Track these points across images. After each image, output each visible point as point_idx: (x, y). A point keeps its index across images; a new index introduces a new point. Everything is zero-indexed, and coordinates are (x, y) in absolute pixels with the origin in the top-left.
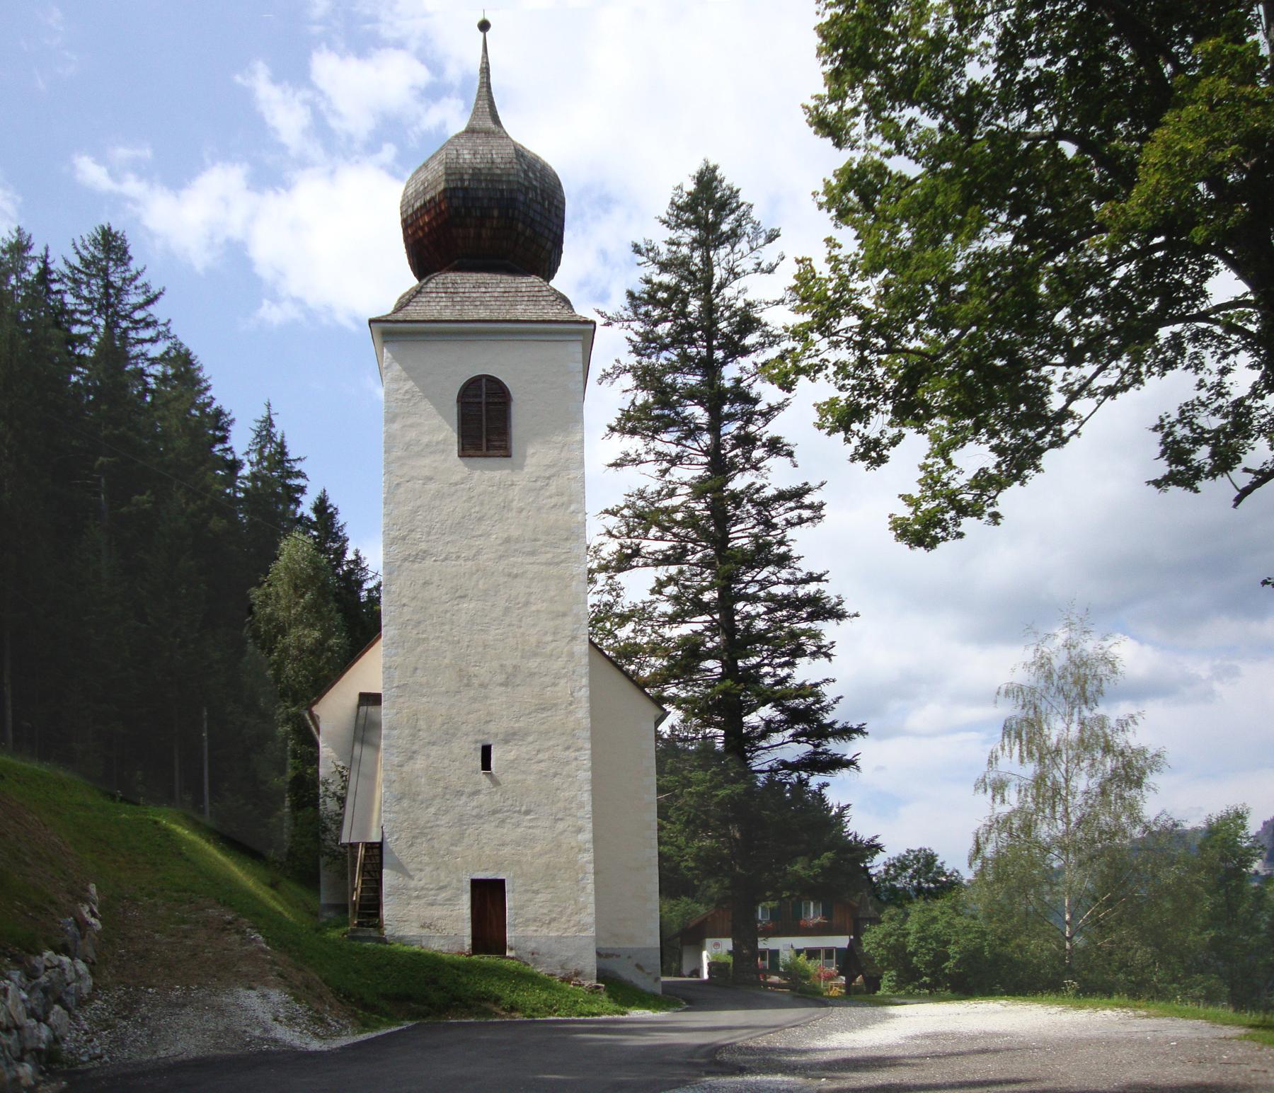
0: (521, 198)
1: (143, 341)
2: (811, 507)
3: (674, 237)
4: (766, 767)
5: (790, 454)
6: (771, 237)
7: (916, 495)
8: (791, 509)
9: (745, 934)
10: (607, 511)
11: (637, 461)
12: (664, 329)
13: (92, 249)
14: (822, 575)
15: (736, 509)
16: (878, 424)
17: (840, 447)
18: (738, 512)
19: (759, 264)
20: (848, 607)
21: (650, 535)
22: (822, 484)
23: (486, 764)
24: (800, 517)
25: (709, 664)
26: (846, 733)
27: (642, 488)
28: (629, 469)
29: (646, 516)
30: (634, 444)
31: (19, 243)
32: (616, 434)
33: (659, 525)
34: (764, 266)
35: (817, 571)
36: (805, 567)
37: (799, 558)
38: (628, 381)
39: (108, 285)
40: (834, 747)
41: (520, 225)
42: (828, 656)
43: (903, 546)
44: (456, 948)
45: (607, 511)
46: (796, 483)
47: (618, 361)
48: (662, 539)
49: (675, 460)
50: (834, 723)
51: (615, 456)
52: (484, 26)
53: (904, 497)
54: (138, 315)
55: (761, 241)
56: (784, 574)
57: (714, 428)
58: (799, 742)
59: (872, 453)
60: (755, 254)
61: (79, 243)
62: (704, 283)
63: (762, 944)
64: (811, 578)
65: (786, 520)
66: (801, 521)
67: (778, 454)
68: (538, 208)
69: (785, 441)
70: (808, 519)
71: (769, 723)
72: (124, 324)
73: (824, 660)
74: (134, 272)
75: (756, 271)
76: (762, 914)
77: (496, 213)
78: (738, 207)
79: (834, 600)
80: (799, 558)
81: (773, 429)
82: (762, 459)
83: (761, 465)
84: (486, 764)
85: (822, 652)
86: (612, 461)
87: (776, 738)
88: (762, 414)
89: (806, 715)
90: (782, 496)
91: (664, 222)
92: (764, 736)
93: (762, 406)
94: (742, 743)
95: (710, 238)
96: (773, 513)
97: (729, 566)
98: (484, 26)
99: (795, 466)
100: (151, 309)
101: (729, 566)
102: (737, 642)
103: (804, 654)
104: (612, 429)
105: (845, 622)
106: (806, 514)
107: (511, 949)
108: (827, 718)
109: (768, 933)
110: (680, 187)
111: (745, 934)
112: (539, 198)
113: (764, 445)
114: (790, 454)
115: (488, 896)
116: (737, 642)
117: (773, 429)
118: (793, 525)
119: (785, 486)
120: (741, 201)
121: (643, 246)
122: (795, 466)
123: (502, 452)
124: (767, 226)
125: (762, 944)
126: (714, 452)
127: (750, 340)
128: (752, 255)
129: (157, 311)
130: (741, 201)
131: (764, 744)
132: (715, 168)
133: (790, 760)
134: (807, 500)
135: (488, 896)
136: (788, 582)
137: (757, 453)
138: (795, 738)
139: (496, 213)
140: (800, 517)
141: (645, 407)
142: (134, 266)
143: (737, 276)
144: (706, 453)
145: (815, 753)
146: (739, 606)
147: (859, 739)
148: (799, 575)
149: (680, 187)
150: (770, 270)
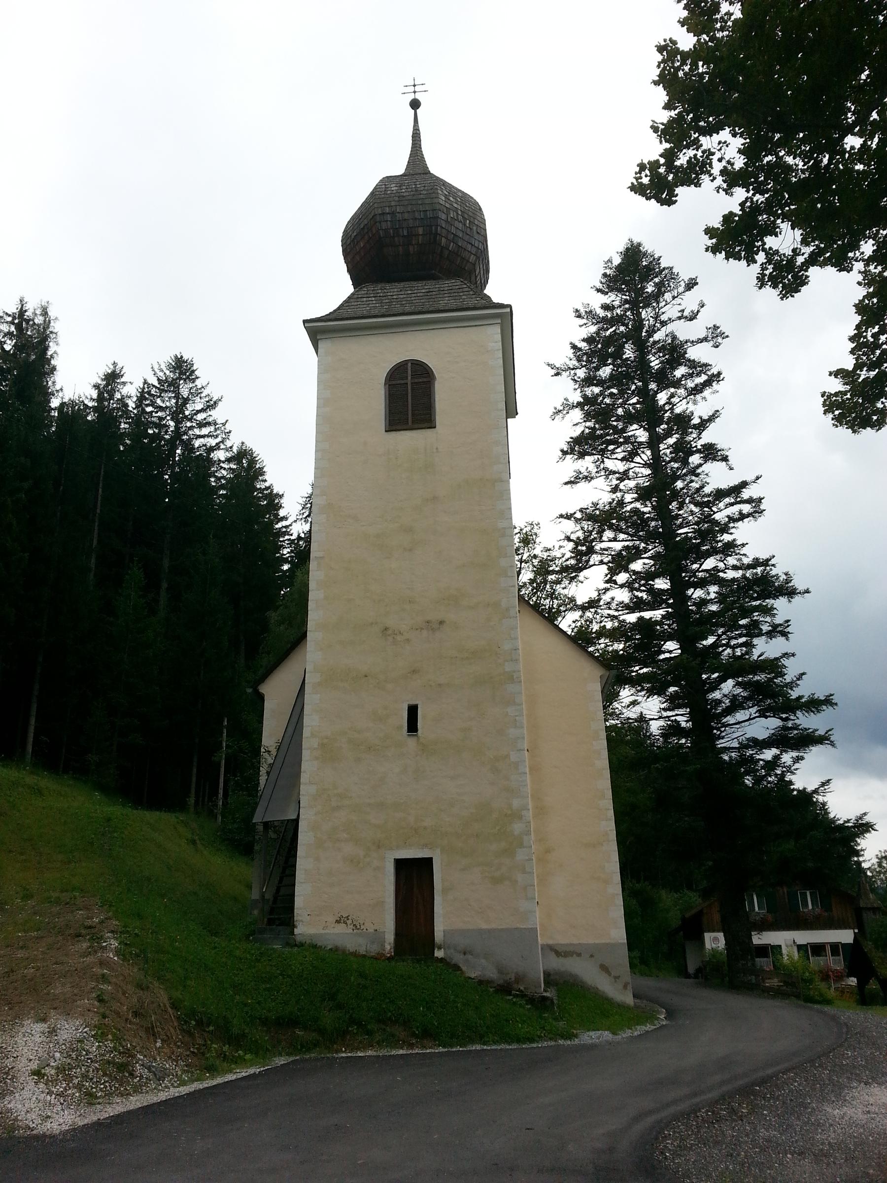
0: (444, 217)
1: (203, 436)
2: (749, 501)
3: (608, 302)
4: (735, 744)
5: (725, 459)
6: (691, 284)
7: (850, 367)
8: (732, 504)
9: (738, 929)
10: (561, 516)
11: (588, 478)
12: (605, 372)
13: (168, 373)
14: (768, 560)
15: (679, 509)
16: (786, 239)
17: (743, 273)
18: (681, 512)
19: (683, 311)
20: (798, 583)
21: (605, 538)
22: (758, 478)
23: (412, 727)
24: (740, 513)
25: (671, 645)
26: (814, 705)
27: (595, 501)
28: (583, 485)
29: (601, 519)
30: (588, 463)
31: (114, 372)
32: (569, 457)
33: (611, 527)
34: (686, 314)
35: (763, 556)
36: (751, 553)
37: (743, 545)
38: (577, 415)
39: (177, 396)
40: (805, 721)
41: (443, 240)
42: (785, 634)
43: (844, 432)
44: (374, 949)
45: (561, 516)
46: (734, 481)
47: (566, 399)
48: (615, 540)
49: (624, 476)
50: (800, 697)
51: (569, 475)
52: (415, 104)
53: (838, 373)
54: (200, 417)
55: (681, 289)
56: (731, 561)
57: (654, 443)
58: (766, 717)
59: (786, 277)
60: (677, 301)
61: (156, 368)
62: (638, 336)
63: (760, 939)
64: (756, 563)
65: (728, 516)
66: (742, 517)
67: (714, 459)
68: (460, 226)
69: (719, 447)
70: (749, 515)
71: (734, 698)
72: (189, 424)
73: (780, 639)
74: (199, 387)
75: (680, 318)
76: (756, 906)
77: (421, 231)
78: (661, 272)
79: (783, 577)
80: (743, 545)
81: (707, 437)
82: (700, 465)
83: (699, 471)
84: (412, 727)
85: (780, 631)
86: (567, 480)
87: (741, 715)
88: (695, 427)
89: (769, 689)
90: (720, 494)
91: (599, 290)
92: (729, 711)
93: (696, 421)
94: (707, 720)
95: (639, 301)
96: (714, 509)
97: (676, 557)
98: (415, 104)
99: (731, 469)
100: (212, 413)
101: (676, 557)
102: (689, 624)
103: (760, 634)
104: (564, 453)
105: (797, 599)
106: (746, 508)
107: (440, 948)
108: (794, 694)
109: (765, 926)
110: (610, 261)
111: (738, 929)
112: (460, 218)
113: (698, 451)
114: (725, 459)
115: (414, 877)
116: (689, 624)
117: (707, 437)
118: (736, 520)
119: (724, 485)
120: (663, 266)
121: (582, 311)
122: (731, 469)
123: (426, 425)
124: (685, 276)
125: (760, 939)
126: (656, 464)
127: (680, 372)
128: (674, 302)
129: (216, 415)
130: (663, 266)
131: (730, 719)
132: (639, 245)
133: (761, 738)
134: (746, 494)
135: (414, 877)
136: (735, 568)
137: (695, 459)
138: (763, 714)
139: (421, 231)
140: (740, 513)
141: (593, 429)
142: (199, 383)
143: (664, 324)
144: (646, 465)
145: (785, 728)
146: (690, 592)
147: (828, 711)
148: (746, 561)
149: (610, 261)
150: (691, 319)
